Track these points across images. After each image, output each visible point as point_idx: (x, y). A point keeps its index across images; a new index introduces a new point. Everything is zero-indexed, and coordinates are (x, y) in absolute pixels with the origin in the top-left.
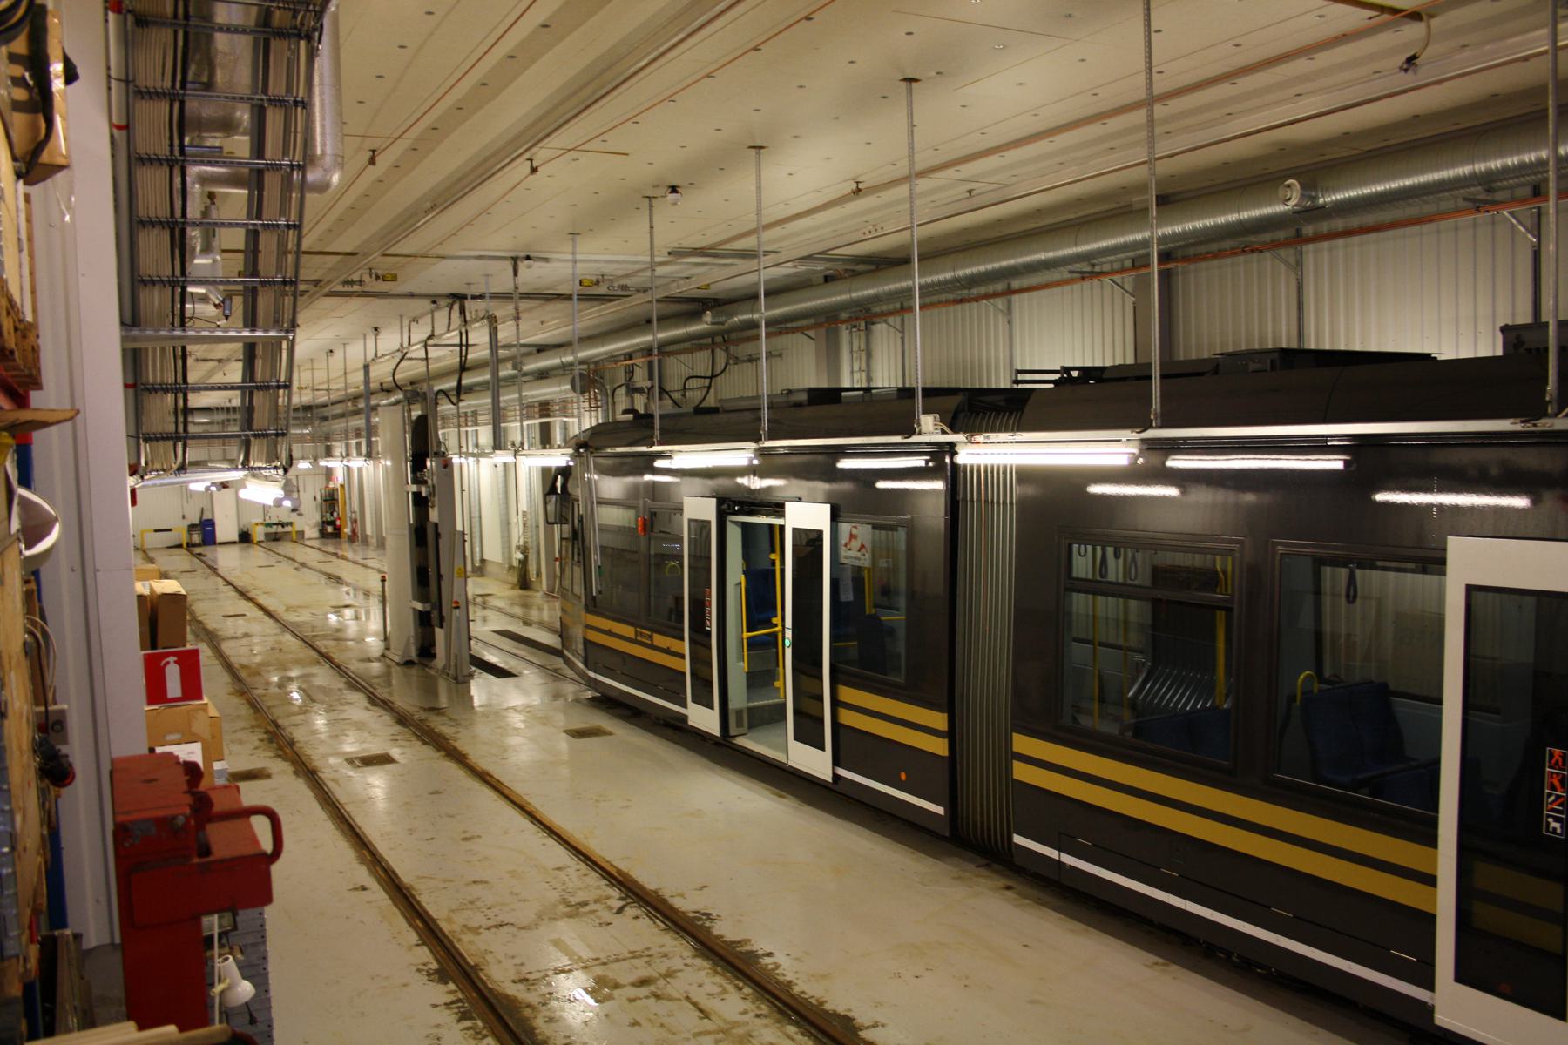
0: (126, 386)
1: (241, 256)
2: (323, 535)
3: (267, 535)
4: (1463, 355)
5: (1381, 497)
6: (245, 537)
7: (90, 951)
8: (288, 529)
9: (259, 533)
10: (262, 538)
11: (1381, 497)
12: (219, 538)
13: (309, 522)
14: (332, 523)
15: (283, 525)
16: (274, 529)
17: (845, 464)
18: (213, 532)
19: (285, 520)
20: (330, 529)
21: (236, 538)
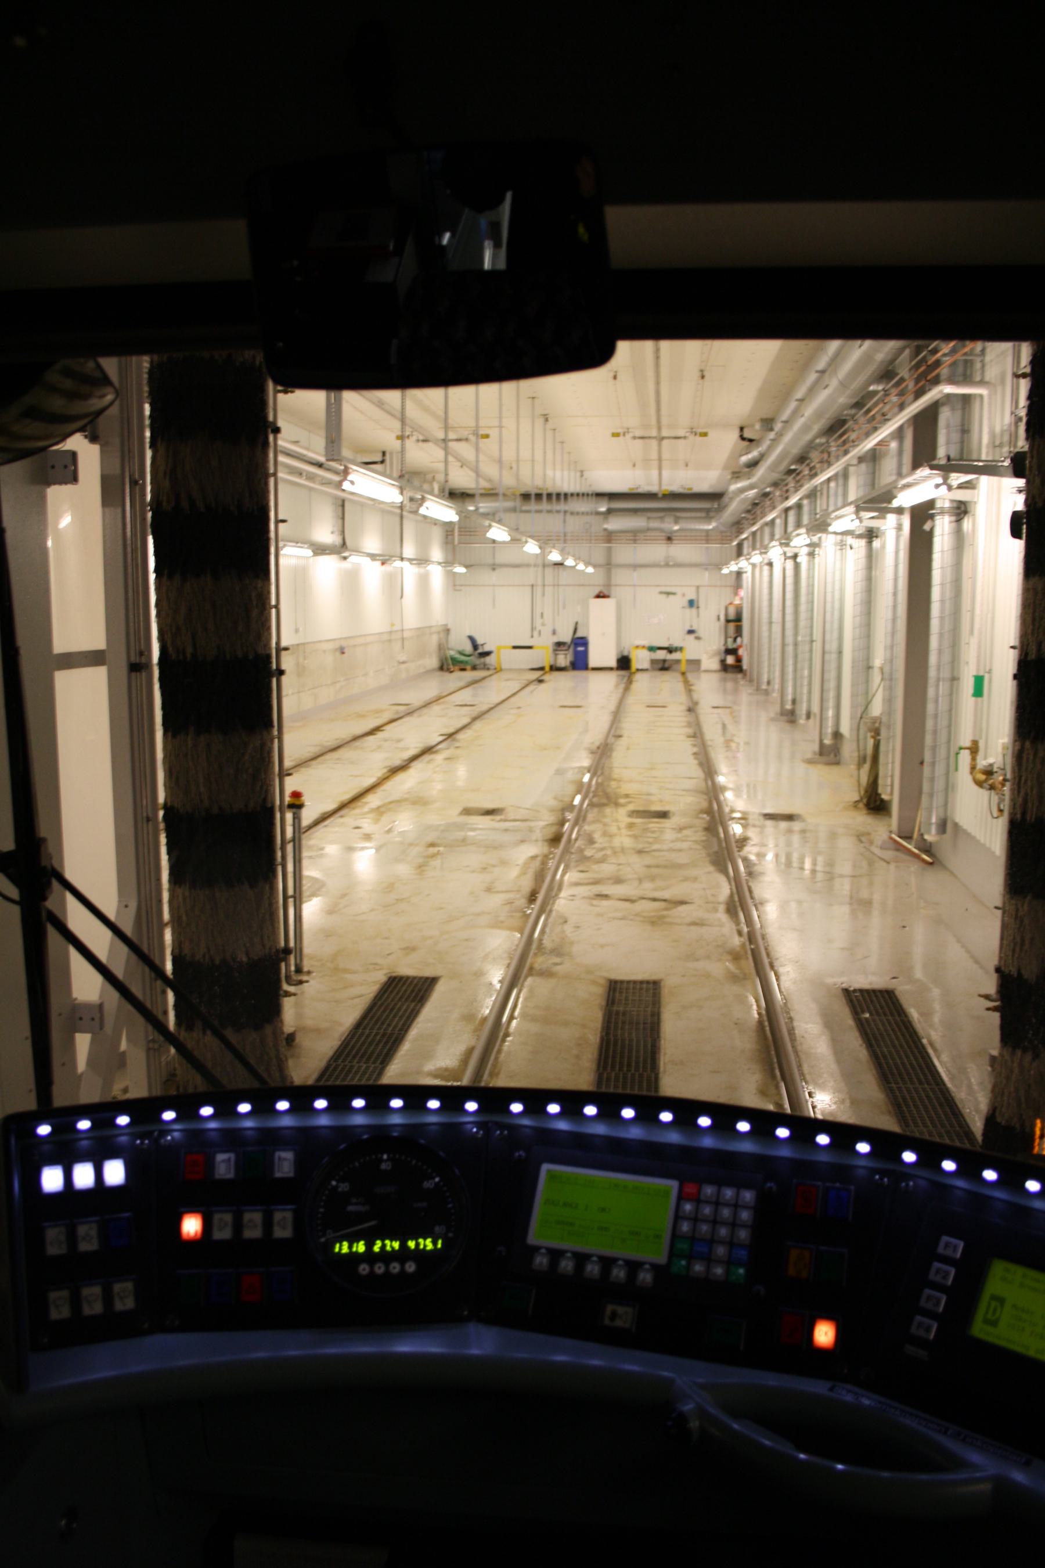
0: (635, 541)
1: (61, 645)
2: (725, 667)
3: (653, 662)
4: (433, 396)
5: (509, 196)
6: (624, 663)
7: (82, 1074)
8: (675, 656)
9: (640, 659)
10: (646, 665)
11: (509, 196)
12: (593, 662)
13: (706, 650)
14: (732, 652)
15: (670, 650)
16: (661, 655)
17: (574, 836)
18: (585, 654)
19: (676, 644)
20: (730, 660)
21: (613, 663)
